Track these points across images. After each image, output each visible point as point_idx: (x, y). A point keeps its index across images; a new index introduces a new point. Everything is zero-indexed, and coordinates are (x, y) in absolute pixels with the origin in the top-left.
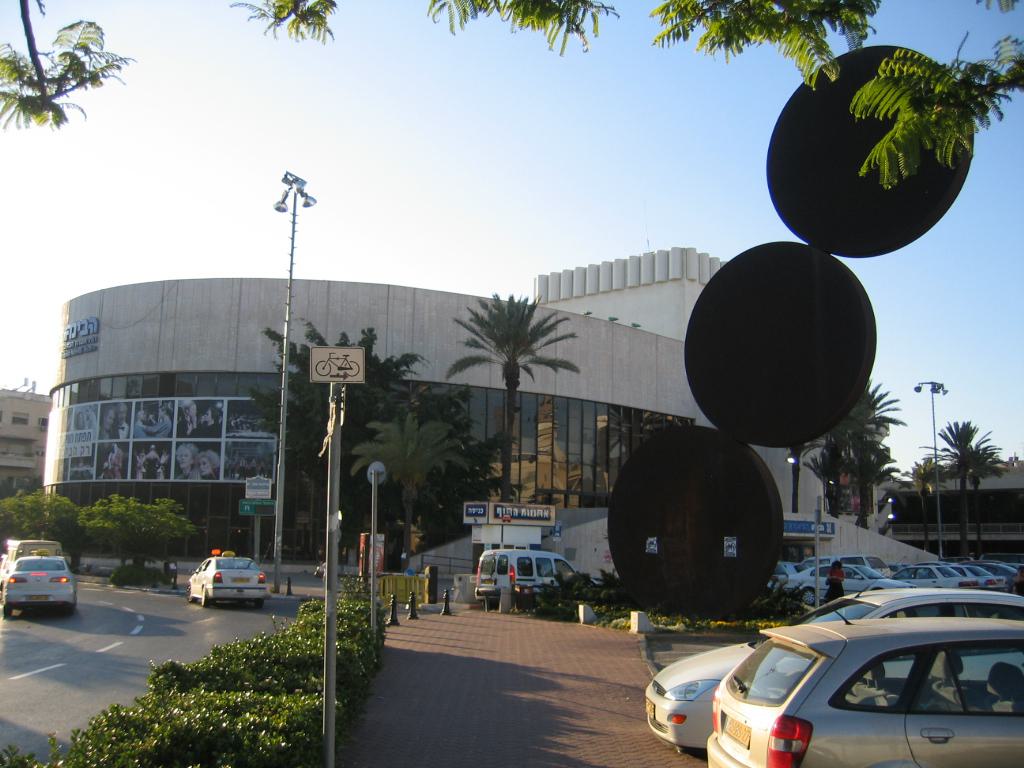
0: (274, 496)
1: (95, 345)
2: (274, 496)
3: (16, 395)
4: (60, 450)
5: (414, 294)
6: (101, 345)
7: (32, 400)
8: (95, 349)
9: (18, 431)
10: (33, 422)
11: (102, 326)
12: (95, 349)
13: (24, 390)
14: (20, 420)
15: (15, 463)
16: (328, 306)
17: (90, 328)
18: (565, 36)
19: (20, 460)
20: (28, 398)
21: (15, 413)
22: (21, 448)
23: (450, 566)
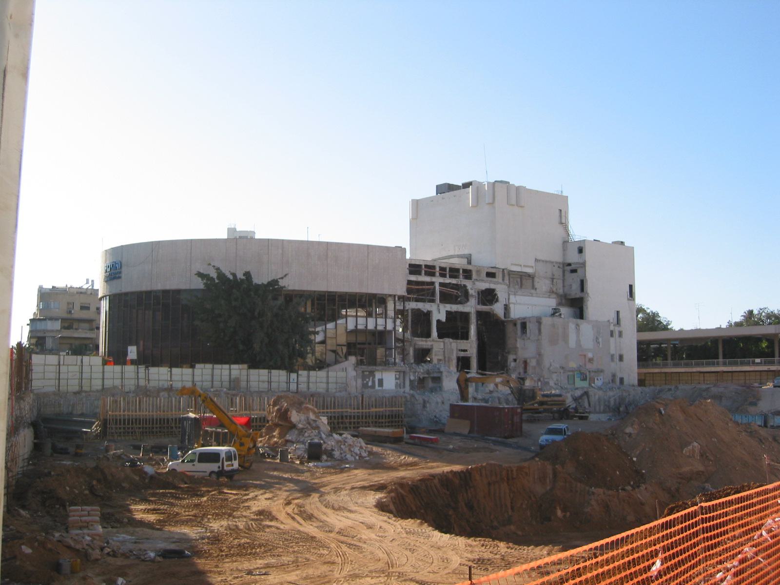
0: (580, 413)
1: (120, 275)
2: (580, 413)
3: (82, 291)
4: (587, 308)
5: (283, 242)
6: (123, 275)
7: (91, 294)
8: (120, 278)
9: (84, 315)
10: (93, 309)
11: (123, 265)
12: (120, 278)
13: (85, 287)
14: (85, 308)
15: (84, 336)
16: (236, 252)
17: (117, 265)
18: (68, 344)
19: (86, 333)
20: (89, 292)
21: (81, 303)
22: (86, 325)
23: (316, 382)
